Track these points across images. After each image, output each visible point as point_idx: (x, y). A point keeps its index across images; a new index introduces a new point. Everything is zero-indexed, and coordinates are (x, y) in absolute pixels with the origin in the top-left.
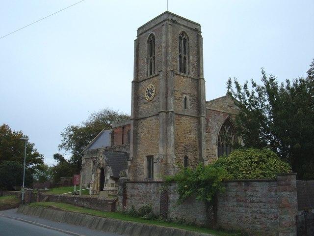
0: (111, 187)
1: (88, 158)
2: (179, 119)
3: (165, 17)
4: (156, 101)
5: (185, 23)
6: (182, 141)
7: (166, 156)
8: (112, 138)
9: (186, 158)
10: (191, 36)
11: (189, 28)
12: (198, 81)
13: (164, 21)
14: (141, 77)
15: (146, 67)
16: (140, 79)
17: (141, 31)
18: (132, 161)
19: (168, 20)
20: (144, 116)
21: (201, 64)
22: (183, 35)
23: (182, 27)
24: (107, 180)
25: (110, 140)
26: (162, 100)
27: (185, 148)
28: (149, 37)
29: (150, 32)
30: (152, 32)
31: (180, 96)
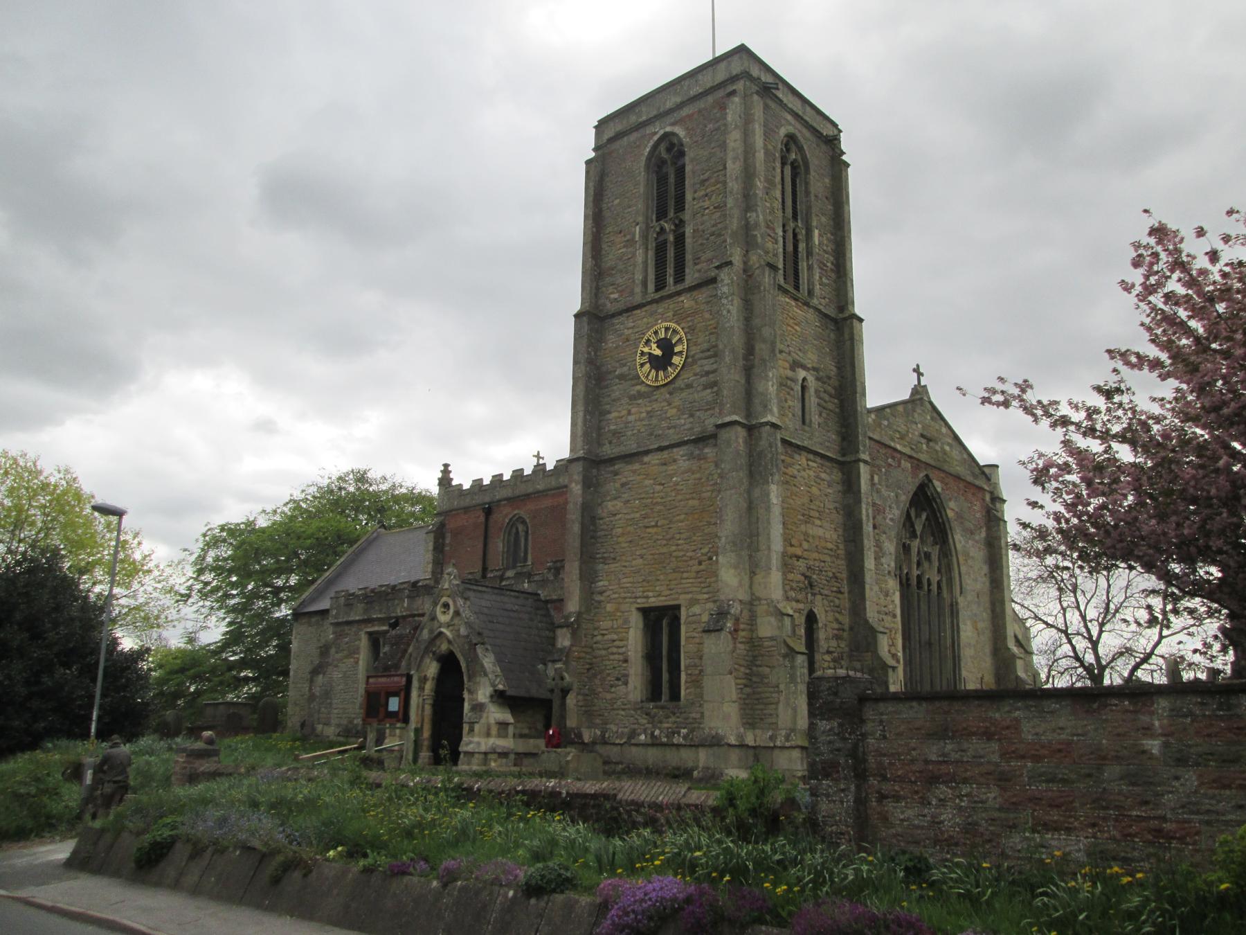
0: (499, 736)
1: (349, 623)
2: (788, 460)
3: (736, 67)
4: (689, 386)
5: (796, 105)
6: (799, 552)
7: (751, 604)
8: (435, 549)
9: (811, 618)
13: (733, 79)
14: (613, 299)
15: (778, 179)
16: (610, 308)
17: (609, 133)
19: (739, 80)
20: (631, 446)
23: (789, 117)
24: (478, 708)
25: (429, 556)
26: (731, 377)
28: (656, 146)
29: (659, 130)
30: (668, 129)
31: (789, 373)
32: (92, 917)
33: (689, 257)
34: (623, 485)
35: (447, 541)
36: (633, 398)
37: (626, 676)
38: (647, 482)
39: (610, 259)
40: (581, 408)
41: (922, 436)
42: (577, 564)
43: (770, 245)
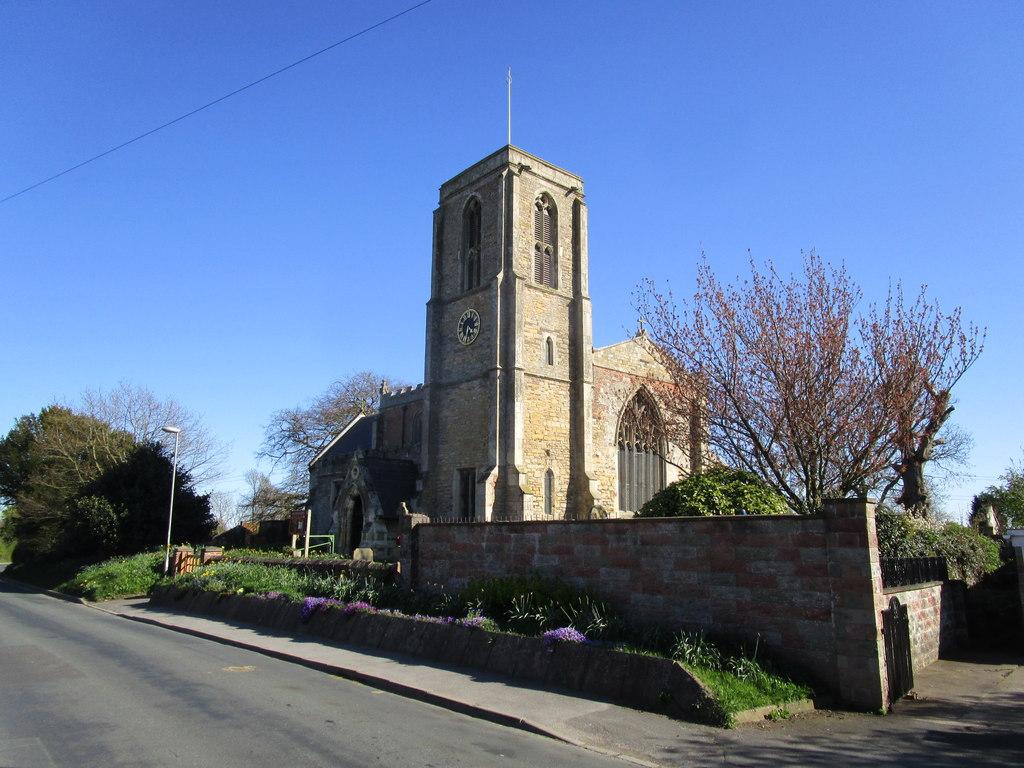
9: (550, 473)
15: (460, 272)
17: (446, 194)
20: (454, 378)
23: (543, 182)
24: (369, 524)
28: (469, 202)
29: (469, 193)
31: (538, 336)
32: (487, 712)
33: (482, 270)
34: (451, 400)
35: (385, 426)
36: (456, 351)
37: (452, 506)
38: (462, 400)
39: (446, 271)
40: (429, 357)
41: (641, 360)
42: (427, 445)
43: (525, 263)
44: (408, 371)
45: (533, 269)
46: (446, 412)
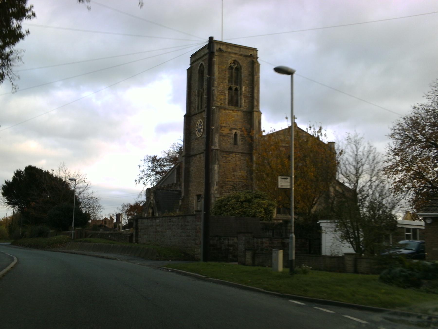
2: (227, 156)
5: (237, 50)
6: (230, 180)
10: (244, 64)
11: (241, 55)
12: (252, 115)
15: (197, 100)
16: (193, 113)
17: (194, 59)
18: (183, 200)
21: (255, 95)
22: (235, 64)
23: (233, 55)
27: (233, 186)
28: (200, 67)
30: (202, 62)
31: (229, 132)
44: (290, 125)
45: (227, 100)
46: (192, 168)
